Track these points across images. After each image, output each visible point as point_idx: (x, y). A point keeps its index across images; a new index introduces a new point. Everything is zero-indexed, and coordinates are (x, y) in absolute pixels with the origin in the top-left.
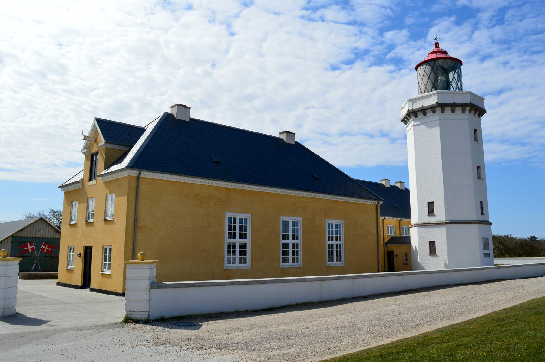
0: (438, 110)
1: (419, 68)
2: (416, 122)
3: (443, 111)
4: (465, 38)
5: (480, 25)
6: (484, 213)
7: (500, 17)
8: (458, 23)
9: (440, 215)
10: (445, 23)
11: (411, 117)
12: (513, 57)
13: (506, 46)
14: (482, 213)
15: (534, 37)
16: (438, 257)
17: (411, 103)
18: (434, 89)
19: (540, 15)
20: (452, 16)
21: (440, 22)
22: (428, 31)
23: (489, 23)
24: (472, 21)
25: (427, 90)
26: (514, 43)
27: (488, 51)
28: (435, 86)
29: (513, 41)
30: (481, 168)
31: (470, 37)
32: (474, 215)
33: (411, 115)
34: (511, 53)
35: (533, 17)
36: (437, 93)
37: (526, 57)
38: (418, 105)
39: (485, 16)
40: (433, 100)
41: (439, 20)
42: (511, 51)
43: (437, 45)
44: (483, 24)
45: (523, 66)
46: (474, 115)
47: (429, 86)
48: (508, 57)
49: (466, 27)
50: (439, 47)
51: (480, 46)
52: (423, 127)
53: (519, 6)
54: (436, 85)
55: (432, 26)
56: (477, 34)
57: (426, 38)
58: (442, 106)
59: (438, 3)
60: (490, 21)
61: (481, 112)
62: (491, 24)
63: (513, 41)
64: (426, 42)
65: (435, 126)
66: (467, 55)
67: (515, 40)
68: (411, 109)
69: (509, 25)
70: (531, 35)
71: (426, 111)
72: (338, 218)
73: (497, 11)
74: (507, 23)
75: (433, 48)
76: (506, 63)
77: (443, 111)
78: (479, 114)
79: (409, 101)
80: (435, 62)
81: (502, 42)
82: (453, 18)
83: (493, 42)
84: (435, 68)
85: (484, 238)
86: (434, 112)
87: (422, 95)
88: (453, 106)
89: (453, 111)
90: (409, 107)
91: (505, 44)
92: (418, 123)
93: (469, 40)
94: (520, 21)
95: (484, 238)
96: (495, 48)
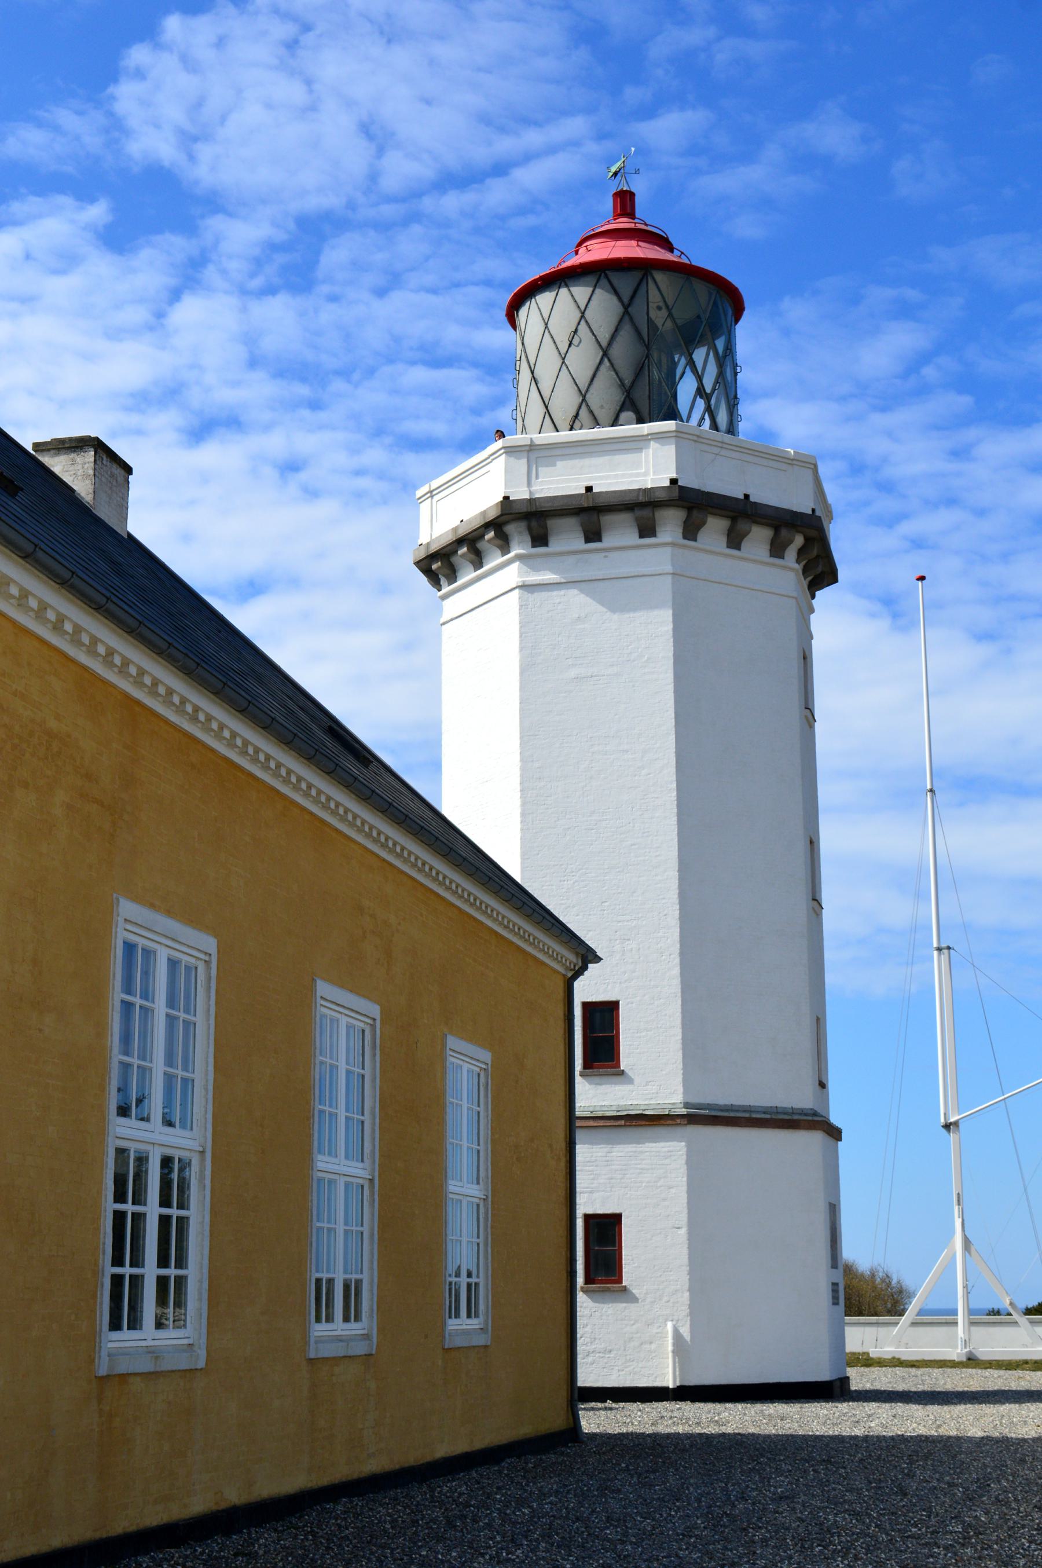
0: (670, 525)
1: (544, 299)
2: (535, 569)
3: (690, 532)
4: (138, 315)
5: (210, 273)
7: (296, 259)
8: (116, 239)
11: (504, 543)
12: (322, 444)
13: (303, 391)
15: (420, 375)
16: (634, 1299)
19: (457, 285)
20: (92, 200)
21: (39, 216)
23: (253, 275)
24: (178, 244)
25: (584, 413)
26: (338, 385)
27: (227, 396)
29: (338, 373)
31: (160, 315)
33: (510, 529)
34: (321, 427)
35: (434, 291)
37: (376, 456)
38: (560, 482)
39: (239, 236)
40: (646, 461)
41: (33, 204)
42: (323, 416)
43: (625, 202)
44: (224, 272)
45: (359, 495)
47: (605, 395)
48: (306, 443)
49: (149, 268)
50: (632, 215)
52: (576, 600)
53: (384, 227)
54: (641, 395)
56: (190, 311)
58: (691, 506)
59: (40, 124)
60: (258, 263)
61: (821, 572)
62: (257, 283)
63: (338, 373)
65: (648, 605)
66: (132, 395)
67: (345, 373)
68: (519, 493)
69: (333, 298)
70: (413, 363)
73: (292, 226)
74: (325, 289)
76: (290, 467)
77: (690, 532)
80: (645, 276)
81: (289, 370)
82: (98, 212)
83: (254, 362)
84: (637, 310)
86: (647, 530)
87: (549, 436)
88: (740, 515)
89: (735, 541)
91: (304, 380)
93: (151, 329)
94: (381, 292)
96: (258, 391)
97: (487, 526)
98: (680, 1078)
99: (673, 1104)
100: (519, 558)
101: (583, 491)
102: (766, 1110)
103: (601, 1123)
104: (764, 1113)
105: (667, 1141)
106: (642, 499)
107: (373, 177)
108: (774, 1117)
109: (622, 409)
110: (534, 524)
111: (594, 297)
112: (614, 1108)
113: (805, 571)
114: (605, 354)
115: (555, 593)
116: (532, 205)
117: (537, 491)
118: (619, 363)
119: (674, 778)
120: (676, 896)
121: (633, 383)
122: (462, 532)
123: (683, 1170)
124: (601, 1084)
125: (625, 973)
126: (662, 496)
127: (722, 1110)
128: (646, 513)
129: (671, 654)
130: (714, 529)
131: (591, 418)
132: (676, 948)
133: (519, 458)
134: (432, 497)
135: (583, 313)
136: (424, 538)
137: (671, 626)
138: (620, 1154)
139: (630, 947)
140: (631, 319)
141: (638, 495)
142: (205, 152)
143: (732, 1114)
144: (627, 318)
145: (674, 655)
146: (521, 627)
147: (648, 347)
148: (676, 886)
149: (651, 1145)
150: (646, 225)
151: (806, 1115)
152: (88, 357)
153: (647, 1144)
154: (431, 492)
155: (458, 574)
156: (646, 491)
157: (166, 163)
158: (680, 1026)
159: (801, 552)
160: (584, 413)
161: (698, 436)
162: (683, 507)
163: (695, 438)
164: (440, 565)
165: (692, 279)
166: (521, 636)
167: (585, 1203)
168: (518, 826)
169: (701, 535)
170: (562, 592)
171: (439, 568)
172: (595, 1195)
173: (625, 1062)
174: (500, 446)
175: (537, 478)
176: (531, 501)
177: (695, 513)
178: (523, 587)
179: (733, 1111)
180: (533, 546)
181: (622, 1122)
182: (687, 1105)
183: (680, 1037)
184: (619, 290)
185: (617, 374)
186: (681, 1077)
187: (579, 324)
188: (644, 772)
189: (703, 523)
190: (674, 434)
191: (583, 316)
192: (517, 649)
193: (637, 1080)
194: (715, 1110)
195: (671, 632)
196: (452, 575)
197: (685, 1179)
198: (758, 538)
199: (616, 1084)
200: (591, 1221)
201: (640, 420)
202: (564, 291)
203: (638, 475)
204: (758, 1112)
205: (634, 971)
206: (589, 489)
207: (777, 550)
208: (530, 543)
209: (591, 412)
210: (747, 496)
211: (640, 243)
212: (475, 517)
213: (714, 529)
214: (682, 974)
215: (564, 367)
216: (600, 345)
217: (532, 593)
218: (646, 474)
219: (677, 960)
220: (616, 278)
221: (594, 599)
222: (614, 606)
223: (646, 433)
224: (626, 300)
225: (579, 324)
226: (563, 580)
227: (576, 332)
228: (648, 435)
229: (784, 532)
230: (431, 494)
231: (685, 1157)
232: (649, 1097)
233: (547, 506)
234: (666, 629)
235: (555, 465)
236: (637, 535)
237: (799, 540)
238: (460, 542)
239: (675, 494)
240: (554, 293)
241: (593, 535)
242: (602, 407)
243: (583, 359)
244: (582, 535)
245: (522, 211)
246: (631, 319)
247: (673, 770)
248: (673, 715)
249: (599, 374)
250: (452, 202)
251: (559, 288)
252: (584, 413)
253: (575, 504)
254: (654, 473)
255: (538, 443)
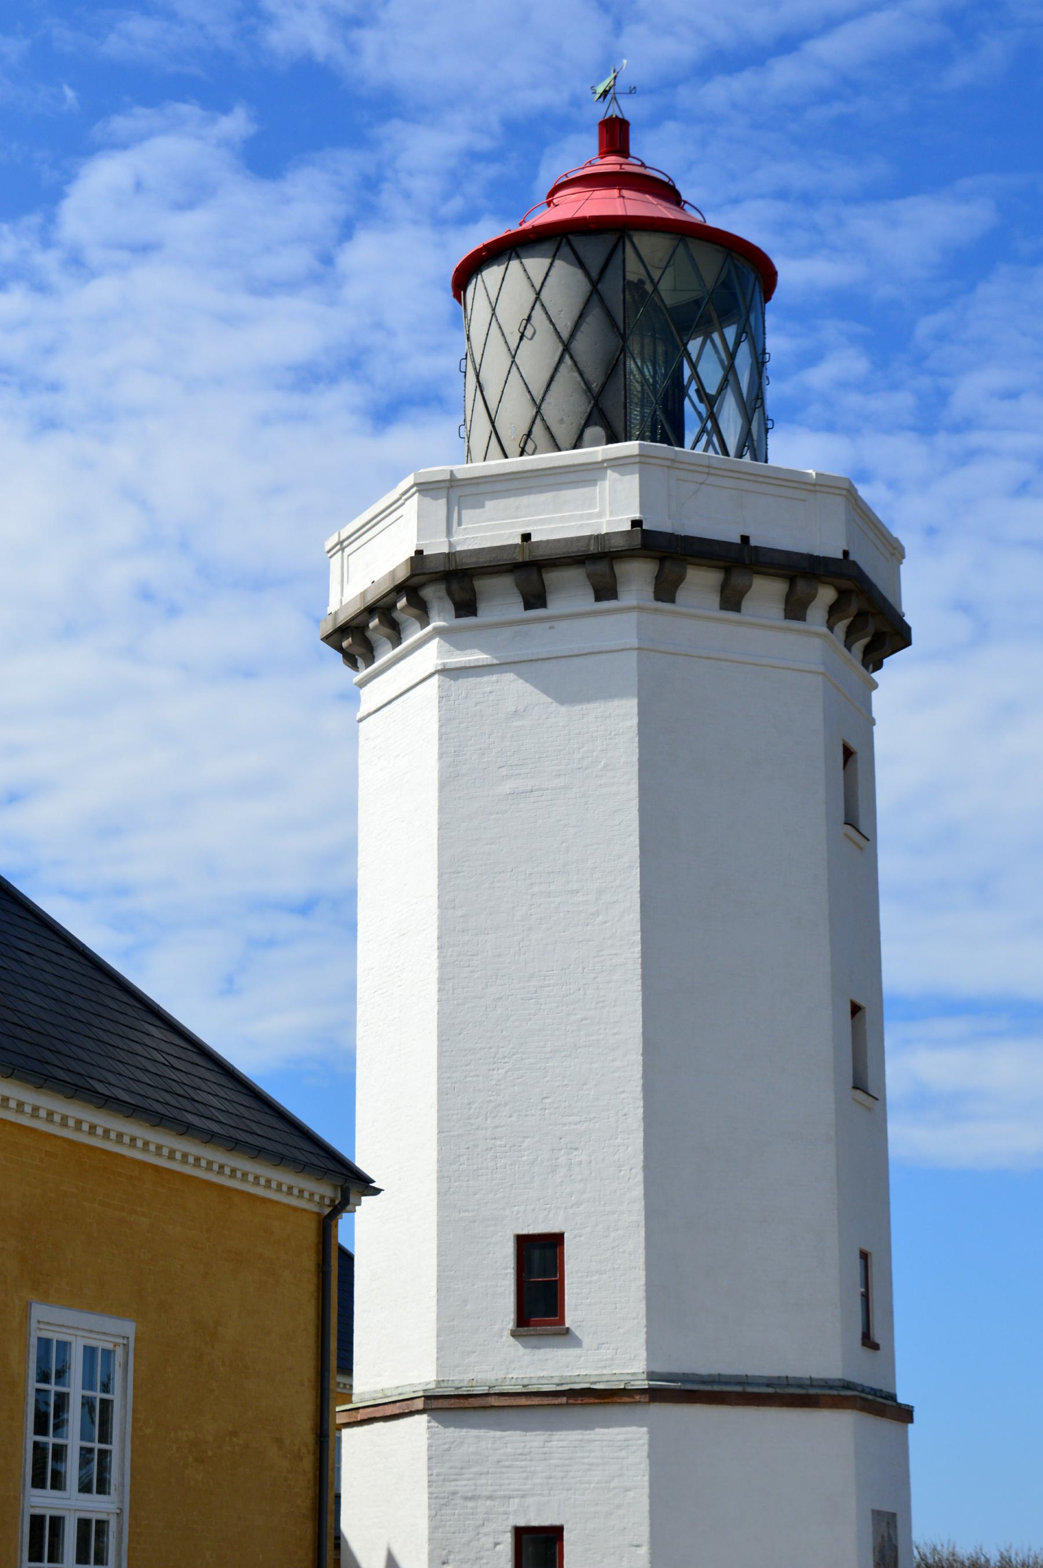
0: (637, 580)
1: (491, 275)
2: (460, 646)
3: (665, 591)
4: (296, 260)
5: (388, 198)
6: (877, 1336)
8: (264, 160)
9: (609, 1333)
10: (176, 146)
11: (422, 610)
14: (868, 1341)
17: (440, 506)
18: (595, 431)
20: (226, 109)
22: (70, 177)
23: (446, 197)
24: (350, 163)
25: (538, 432)
28: (603, 418)
30: (869, 1014)
31: (327, 260)
32: (823, 1353)
33: (428, 593)
36: (642, 460)
38: (489, 529)
39: (424, 149)
40: (604, 498)
41: (141, 118)
43: (615, 135)
44: (407, 195)
46: (848, 645)
47: (565, 405)
49: (309, 198)
50: (624, 152)
51: (379, 326)
52: (512, 688)
54: (612, 405)
55: (90, 150)
56: (364, 252)
57: (51, 219)
58: (664, 555)
59: (148, 12)
62: (456, 204)
64: (47, 243)
68: (437, 546)
71: (481, 584)
72: (98, 1302)
75: (583, 153)
77: (665, 591)
78: (867, 650)
79: (425, 488)
82: (236, 124)
84: (612, 288)
85: (877, 1514)
86: (605, 591)
87: (496, 464)
88: (738, 565)
89: (731, 600)
90: (422, 532)
92: (476, 657)
93: (315, 279)
95: (877, 1514)
97: (399, 589)
98: (642, 1338)
99: (633, 1374)
100: (438, 632)
101: (518, 540)
102: (770, 1382)
103: (536, 1401)
104: (768, 1385)
105: (623, 1426)
106: (593, 549)
107: (608, 62)
108: (779, 1391)
109: (587, 424)
110: (455, 586)
111: (553, 270)
112: (556, 1381)
113: (850, 637)
114: (566, 348)
115: (485, 679)
116: (846, 85)
117: (458, 543)
118: (583, 360)
119: (638, 927)
120: (640, 1089)
121: (603, 387)
122: (370, 599)
123: (645, 1465)
124: (539, 1348)
125: (571, 1194)
126: (619, 544)
127: (704, 1383)
128: (601, 567)
129: (635, 758)
130: (700, 584)
131: (549, 436)
132: (639, 1160)
133: (435, 498)
134: (343, 549)
135: (538, 294)
136: (333, 607)
137: (635, 721)
138: (561, 1444)
139: (577, 1159)
140: (602, 300)
141: (588, 545)
142: (369, 39)
143: (716, 1388)
144: (595, 298)
145: (639, 760)
146: (440, 727)
147: (624, 337)
148: (640, 1075)
149: (606, 1431)
150: (643, 165)
151: (831, 1388)
152: (229, 320)
153: (597, 1430)
154: (341, 543)
155: (376, 654)
156: (598, 538)
157: (320, 57)
158: (643, 1267)
159: (834, 611)
160: (538, 430)
161: (672, 460)
162: (652, 558)
163: (668, 463)
164: (357, 639)
165: (689, 240)
166: (440, 739)
167: (515, 1512)
168: (435, 996)
169: (681, 595)
170: (494, 678)
171: (350, 645)
172: (530, 1500)
173: (570, 1319)
174: (412, 483)
175: (460, 524)
176: (449, 556)
177: (668, 564)
178: (445, 672)
179: (719, 1383)
180: (458, 616)
181: (564, 1400)
182: (651, 1376)
183: (643, 1282)
184: (585, 261)
185: (581, 374)
186: (644, 1336)
187: (533, 308)
188: (600, 919)
189: (680, 579)
190: (637, 459)
191: (538, 298)
192: (436, 757)
193: (586, 1341)
194: (693, 1382)
195: (635, 729)
196: (369, 653)
197: (646, 1478)
198: (766, 594)
199: (558, 1347)
200: (525, 1537)
201: (612, 438)
202: (514, 264)
203: (590, 516)
204: (758, 1385)
205: (584, 1192)
206: (526, 537)
207: (795, 609)
208: (453, 612)
209: (548, 428)
210: (745, 539)
211: (625, 192)
212: (384, 578)
213: (700, 584)
214: (647, 1196)
215: (514, 368)
216: (560, 337)
217: (455, 679)
218: (600, 515)
219: (640, 1177)
220: (577, 241)
221: (535, 686)
222: (565, 697)
223: (600, 459)
224: (595, 275)
225: (533, 308)
226: (495, 662)
227: (529, 319)
228: (603, 461)
229: (801, 585)
230: (341, 545)
231: (646, 1447)
232: (602, 1364)
233: (470, 563)
234: (629, 723)
235: (483, 506)
236: (592, 597)
237: (826, 595)
238: (371, 610)
239: (637, 541)
240: (503, 267)
241: (535, 599)
242: (562, 421)
243: (538, 356)
244: (521, 599)
245: (824, 97)
246: (602, 300)
247: (636, 916)
248: (637, 842)
249: (559, 377)
250: (719, 92)
251: (509, 260)
252: (538, 430)
253: (506, 558)
254: (611, 513)
255: (459, 476)
